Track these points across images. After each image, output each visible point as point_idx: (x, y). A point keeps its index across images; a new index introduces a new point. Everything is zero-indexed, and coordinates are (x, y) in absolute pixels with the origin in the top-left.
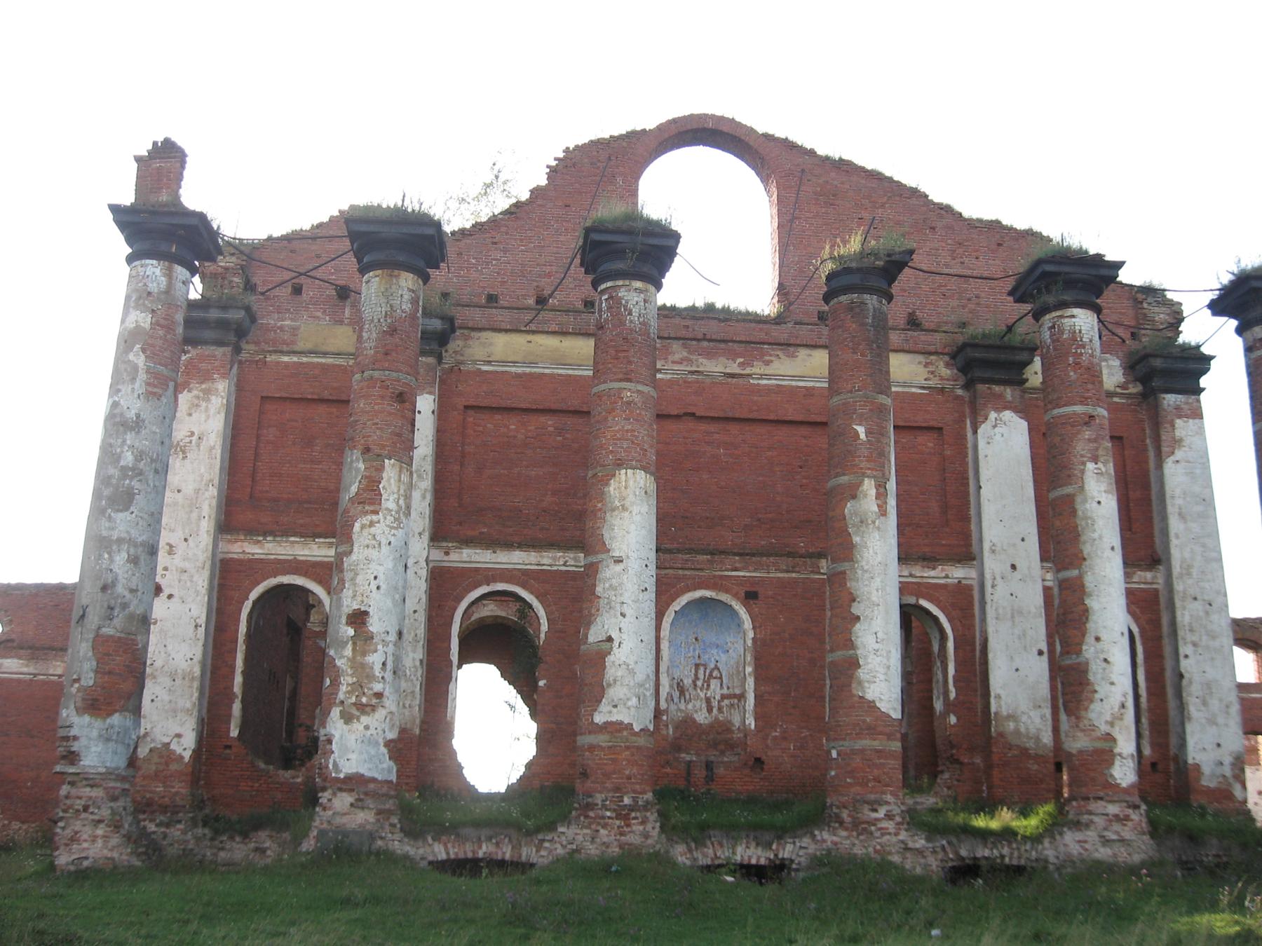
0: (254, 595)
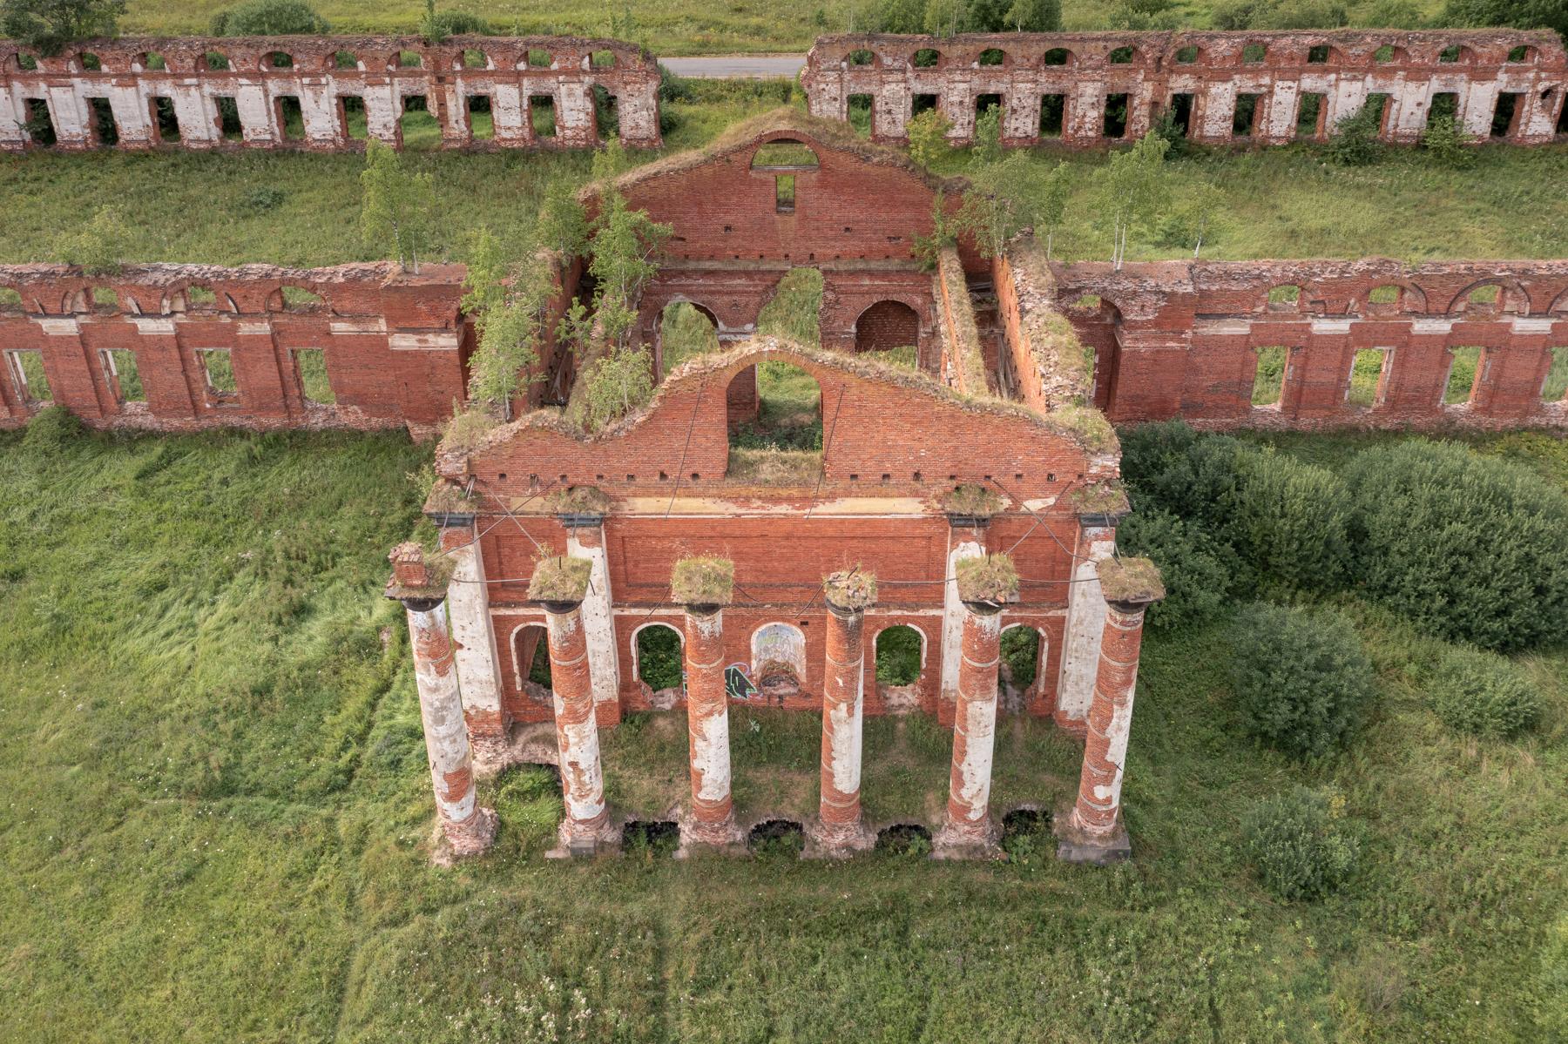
0: (516, 631)
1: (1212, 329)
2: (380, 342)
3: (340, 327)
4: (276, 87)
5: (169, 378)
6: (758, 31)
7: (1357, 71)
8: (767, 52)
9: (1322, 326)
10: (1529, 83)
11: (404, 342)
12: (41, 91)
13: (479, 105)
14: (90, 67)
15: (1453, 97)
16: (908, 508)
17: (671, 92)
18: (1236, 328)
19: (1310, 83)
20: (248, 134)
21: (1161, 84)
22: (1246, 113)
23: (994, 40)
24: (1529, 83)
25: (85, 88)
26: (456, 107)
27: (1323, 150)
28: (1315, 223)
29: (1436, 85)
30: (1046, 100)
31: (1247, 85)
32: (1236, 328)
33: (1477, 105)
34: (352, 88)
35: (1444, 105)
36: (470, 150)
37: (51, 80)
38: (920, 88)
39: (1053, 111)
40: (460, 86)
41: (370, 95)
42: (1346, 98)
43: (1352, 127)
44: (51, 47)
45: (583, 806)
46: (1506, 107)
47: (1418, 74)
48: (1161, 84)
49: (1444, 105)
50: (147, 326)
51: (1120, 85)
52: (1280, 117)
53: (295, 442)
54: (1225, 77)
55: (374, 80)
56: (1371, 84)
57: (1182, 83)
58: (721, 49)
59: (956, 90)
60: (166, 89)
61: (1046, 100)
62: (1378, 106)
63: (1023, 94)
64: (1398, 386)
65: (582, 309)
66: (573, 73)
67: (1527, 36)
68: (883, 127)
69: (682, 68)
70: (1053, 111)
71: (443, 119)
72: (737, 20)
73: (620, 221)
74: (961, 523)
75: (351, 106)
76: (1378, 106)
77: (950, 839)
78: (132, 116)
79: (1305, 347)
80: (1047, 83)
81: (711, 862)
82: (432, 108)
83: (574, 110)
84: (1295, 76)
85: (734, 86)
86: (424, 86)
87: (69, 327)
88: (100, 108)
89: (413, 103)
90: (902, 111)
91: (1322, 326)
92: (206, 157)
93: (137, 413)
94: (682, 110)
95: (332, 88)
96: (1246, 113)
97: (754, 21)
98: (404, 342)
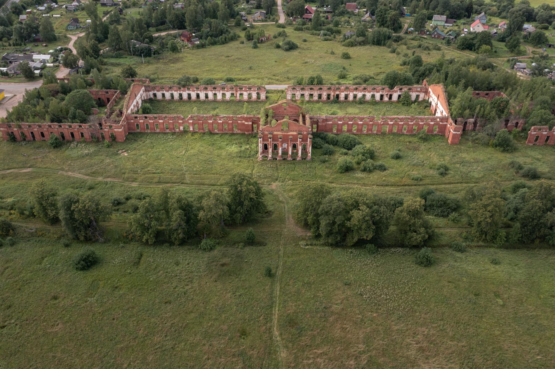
1: (328, 123)
2: (244, 124)
3: (239, 122)
4: (214, 92)
5: (220, 127)
6: (278, 80)
7: (361, 91)
8: (280, 84)
9: (339, 122)
10: (385, 93)
11: (246, 123)
12: (181, 92)
13: (241, 94)
14: (189, 89)
15: (374, 95)
16: (295, 133)
17: (267, 92)
18: (331, 123)
19: (355, 93)
20: (209, 99)
21: (335, 93)
22: (346, 97)
23: (312, 86)
24: (385, 93)
25: (188, 92)
26: (238, 95)
27: (356, 103)
28: (350, 112)
29: (372, 93)
30: (319, 95)
31: (346, 93)
32: (331, 123)
33: (378, 96)
34: (224, 92)
35: (373, 96)
36: (240, 101)
37: (183, 91)
38: (302, 93)
39: (320, 96)
40: (239, 92)
41: (227, 93)
42: (360, 95)
43: (360, 99)
44: (184, 86)
45: (270, 156)
46: (382, 96)
47: (369, 92)
48: (335, 93)
49: (373, 96)
50: (219, 121)
51: (329, 93)
52: (351, 98)
53: (233, 134)
54: (343, 92)
55: (227, 91)
56: (363, 93)
57: (337, 93)
58: (272, 84)
59: (307, 93)
60: (199, 92)
61: (319, 95)
62: (364, 96)
63: (316, 94)
64: (348, 129)
65: (34, 210)
66: (255, 91)
67: (384, 86)
68: (297, 98)
69: (268, 87)
70: (320, 96)
71: (236, 97)
72: (274, 77)
73: (271, 111)
74: (299, 134)
75: (224, 95)
76: (364, 96)
77: (298, 159)
78: (194, 96)
79: (338, 125)
80: (319, 93)
81: (279, 160)
82: (235, 95)
83: (254, 96)
84: (353, 92)
85: (275, 91)
86: (234, 92)
87: (211, 121)
88: (189, 95)
89: (232, 94)
90: (299, 96)
91: (339, 122)
92: (204, 102)
93: (216, 131)
94: (269, 95)
95: (221, 92)
96: (346, 97)
97: (277, 78)
98: (246, 123)
